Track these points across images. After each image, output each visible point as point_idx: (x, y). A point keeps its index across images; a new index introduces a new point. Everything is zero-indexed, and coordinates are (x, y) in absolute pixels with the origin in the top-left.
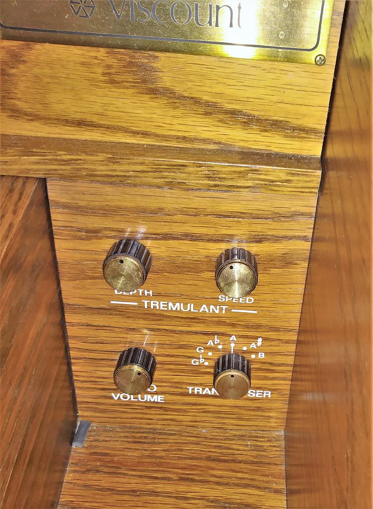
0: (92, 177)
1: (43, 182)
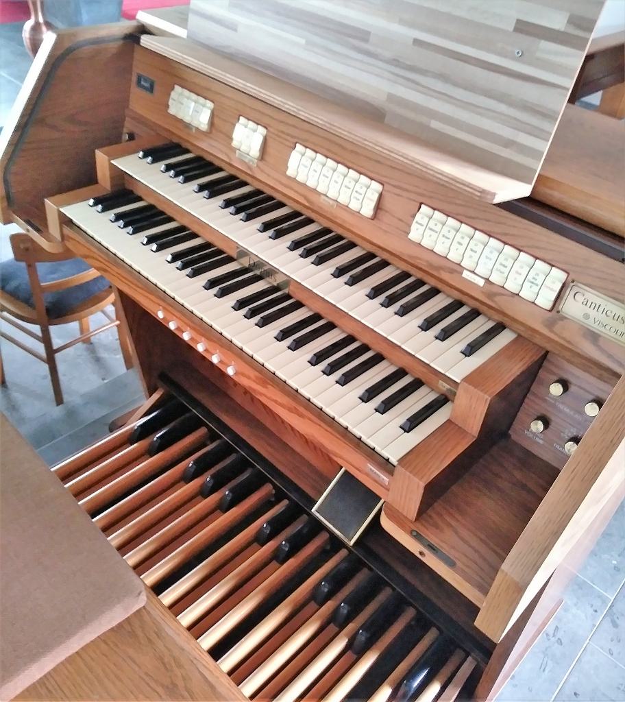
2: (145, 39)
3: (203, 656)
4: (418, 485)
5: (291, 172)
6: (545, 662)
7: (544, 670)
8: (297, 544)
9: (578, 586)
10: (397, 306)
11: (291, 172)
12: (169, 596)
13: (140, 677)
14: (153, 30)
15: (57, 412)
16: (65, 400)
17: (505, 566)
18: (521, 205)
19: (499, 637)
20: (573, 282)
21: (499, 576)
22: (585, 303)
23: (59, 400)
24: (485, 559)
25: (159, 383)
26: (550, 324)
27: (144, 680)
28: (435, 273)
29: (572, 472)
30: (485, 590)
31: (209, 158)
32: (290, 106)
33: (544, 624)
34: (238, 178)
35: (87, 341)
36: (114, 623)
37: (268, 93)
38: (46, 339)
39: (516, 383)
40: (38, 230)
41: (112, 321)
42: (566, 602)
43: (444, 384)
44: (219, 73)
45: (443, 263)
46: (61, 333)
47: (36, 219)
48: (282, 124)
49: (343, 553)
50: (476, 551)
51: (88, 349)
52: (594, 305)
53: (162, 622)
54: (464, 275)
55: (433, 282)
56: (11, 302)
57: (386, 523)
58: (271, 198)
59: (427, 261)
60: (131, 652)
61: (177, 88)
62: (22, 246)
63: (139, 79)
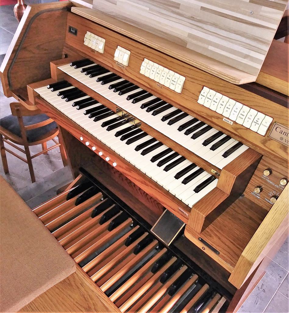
0: (270, 158)
1: (263, 155)
2: (73, 8)
3: (102, 294)
4: (202, 217)
5: (142, 72)
6: (257, 300)
7: (257, 304)
8: (143, 245)
9: (272, 265)
10: (191, 135)
11: (142, 72)
12: (86, 268)
13: (74, 304)
14: (77, 5)
15: (33, 185)
16: (36, 180)
17: (243, 254)
18: (250, 85)
19: (239, 286)
20: (275, 122)
21: (240, 258)
22: (281, 132)
23: (33, 180)
24: (232, 250)
25: (80, 172)
26: (264, 142)
27: (76, 305)
28: (210, 119)
29: (275, 210)
30: (233, 265)
31: (102, 65)
32: (142, 39)
33: (257, 283)
34: (117, 75)
35: (46, 153)
36: (62, 279)
37: (132, 34)
38: (27, 152)
39: (247, 171)
40: (23, 100)
41: (57, 144)
42: (267, 273)
43: (214, 171)
44: (109, 25)
45: (214, 114)
46: (34, 149)
47: (22, 94)
48: (138, 49)
49: (165, 250)
50: (229, 247)
51: (46, 157)
52: (285, 133)
53: (83, 279)
54: (223, 120)
55: (209, 123)
56: (10, 134)
57: (187, 235)
58: (132, 84)
59: (206, 113)
60: (69, 292)
61: (89, 33)
62: (16, 108)
63: (70, 28)
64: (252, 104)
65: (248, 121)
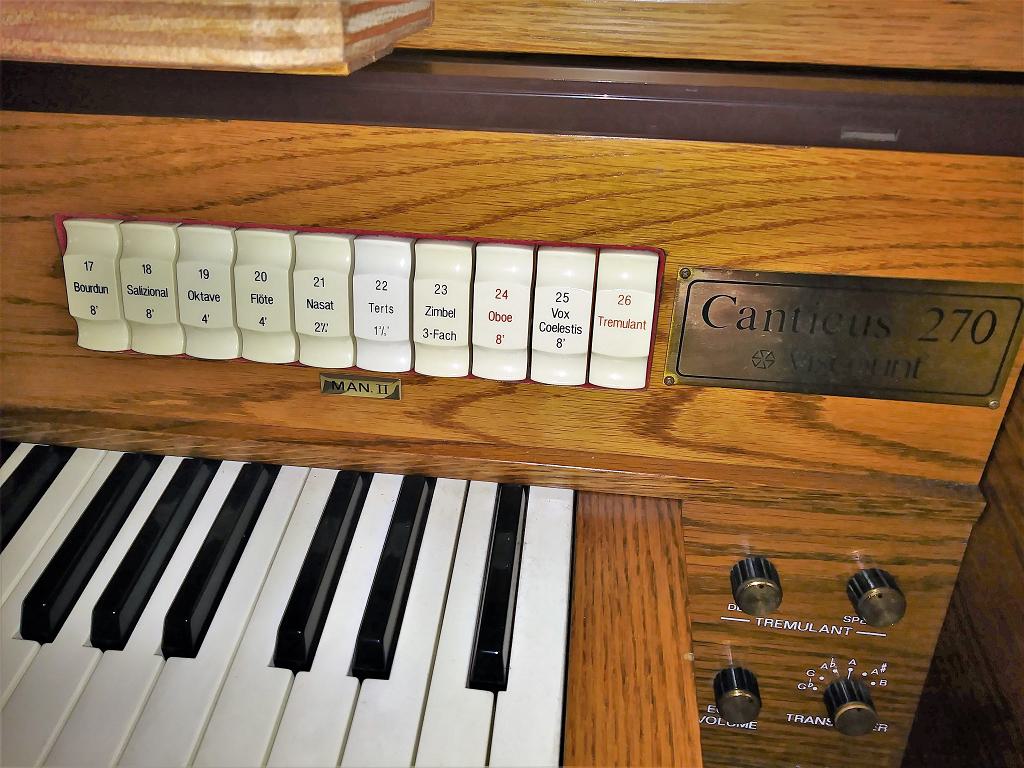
22: (745, 323)
64: (473, 211)
65: (499, 338)
